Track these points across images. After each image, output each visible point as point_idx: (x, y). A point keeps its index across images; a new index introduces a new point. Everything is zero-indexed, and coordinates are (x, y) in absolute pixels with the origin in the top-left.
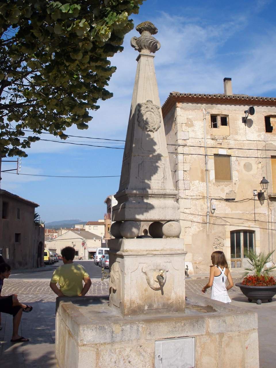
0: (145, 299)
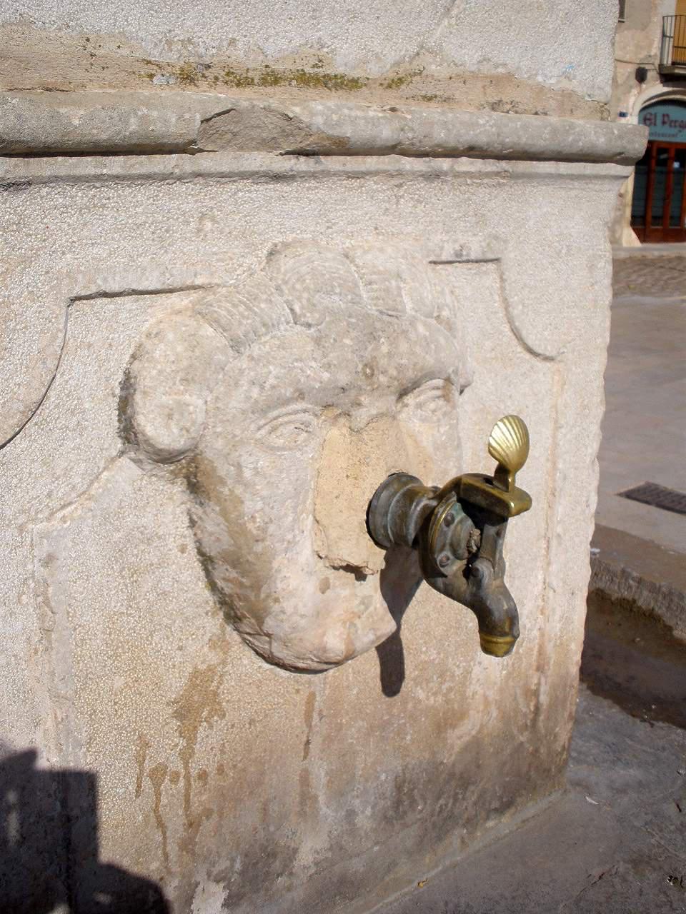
0: (192, 825)
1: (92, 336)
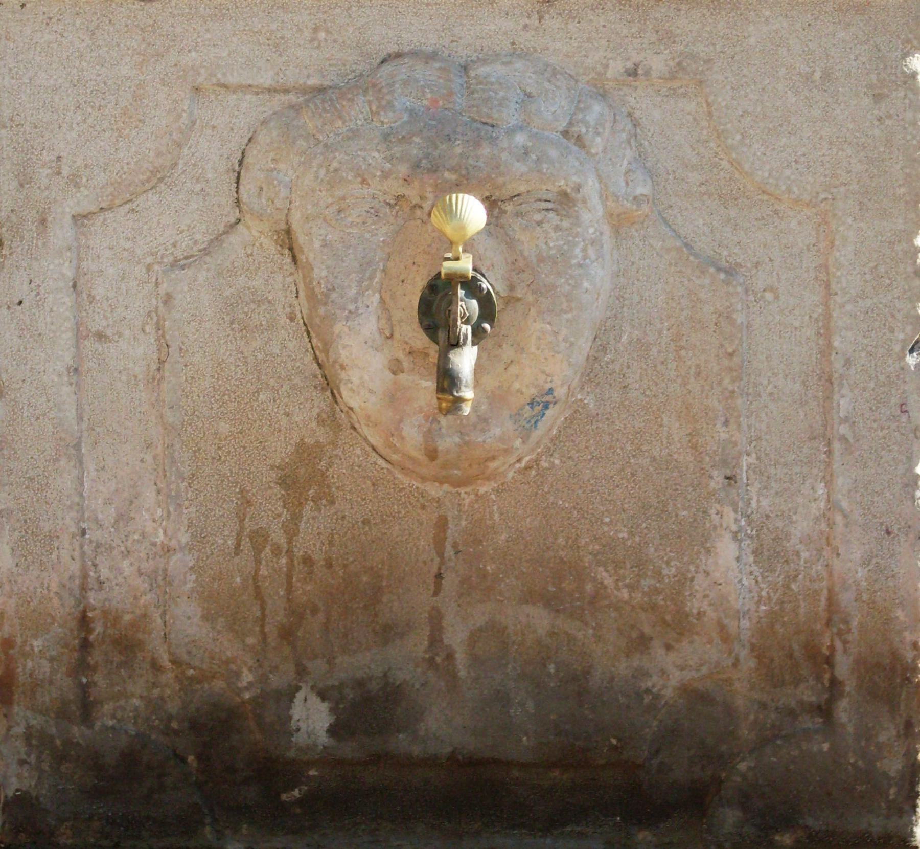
1: (216, 119)
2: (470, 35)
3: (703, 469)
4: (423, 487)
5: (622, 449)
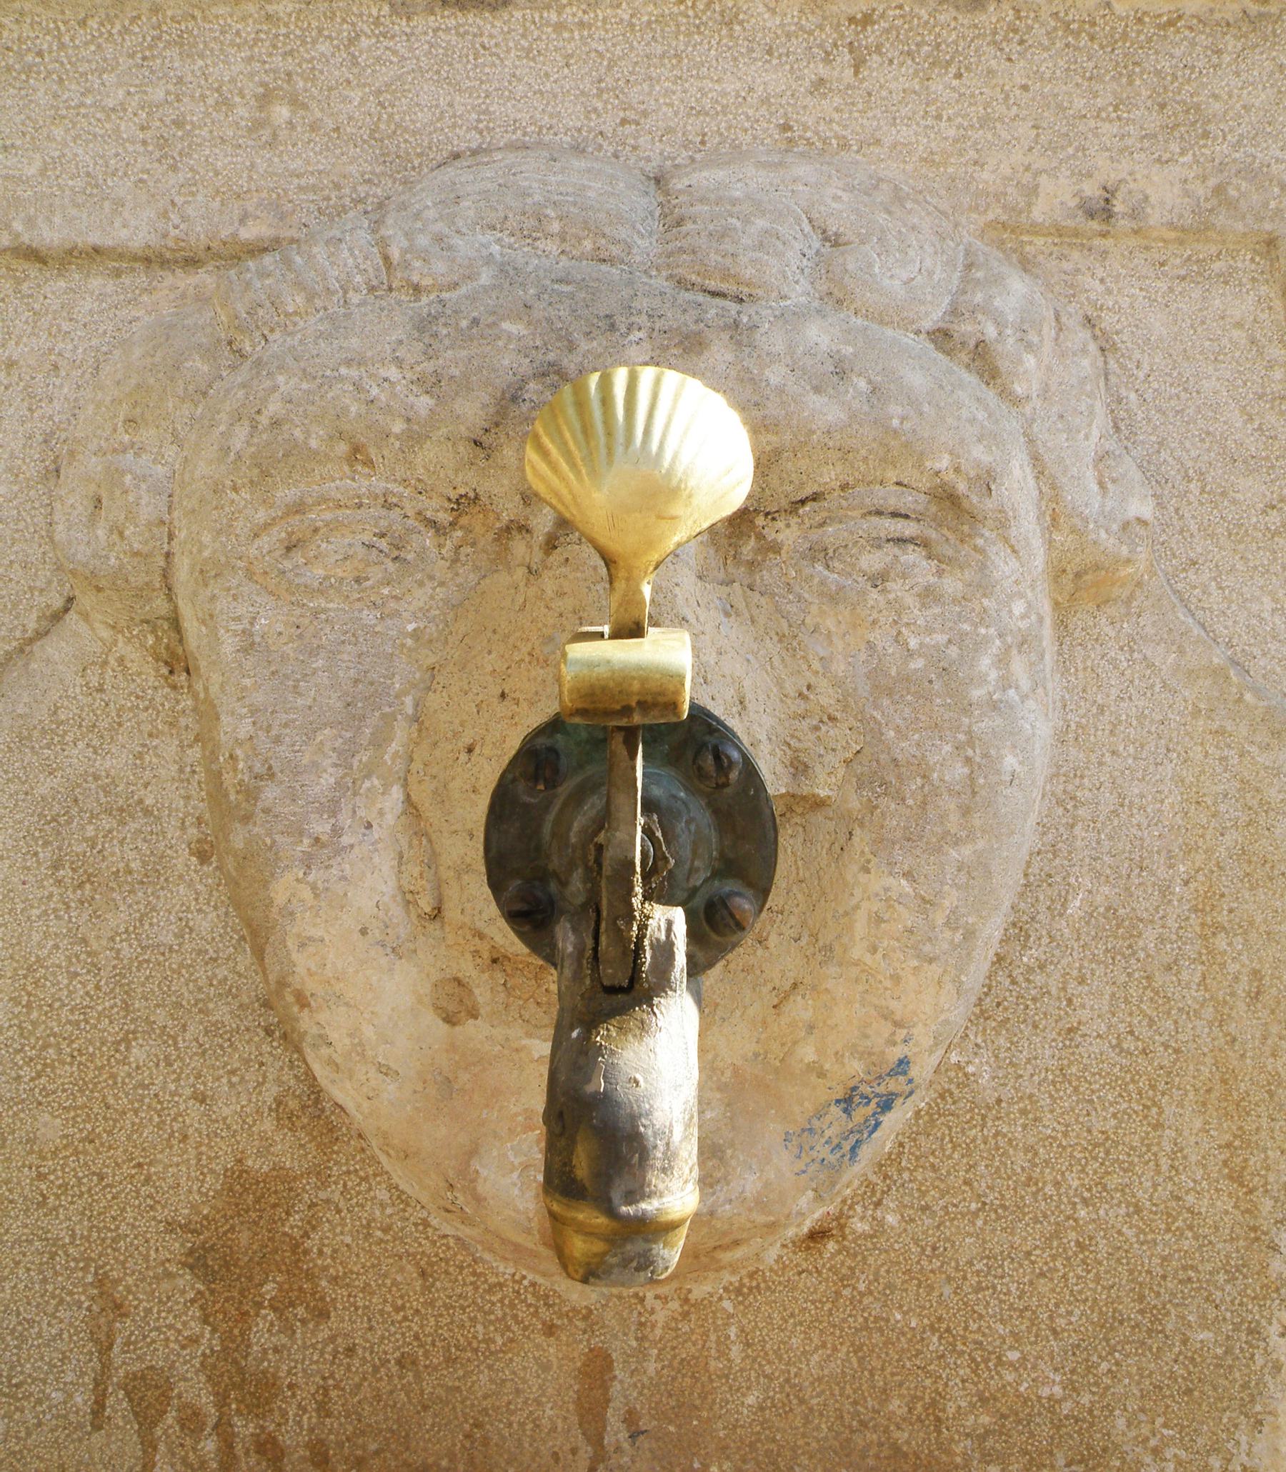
1: (17, 344)
2: (671, 105)
3: (1254, 1229)
4: (548, 1284)
5: (1057, 1184)
